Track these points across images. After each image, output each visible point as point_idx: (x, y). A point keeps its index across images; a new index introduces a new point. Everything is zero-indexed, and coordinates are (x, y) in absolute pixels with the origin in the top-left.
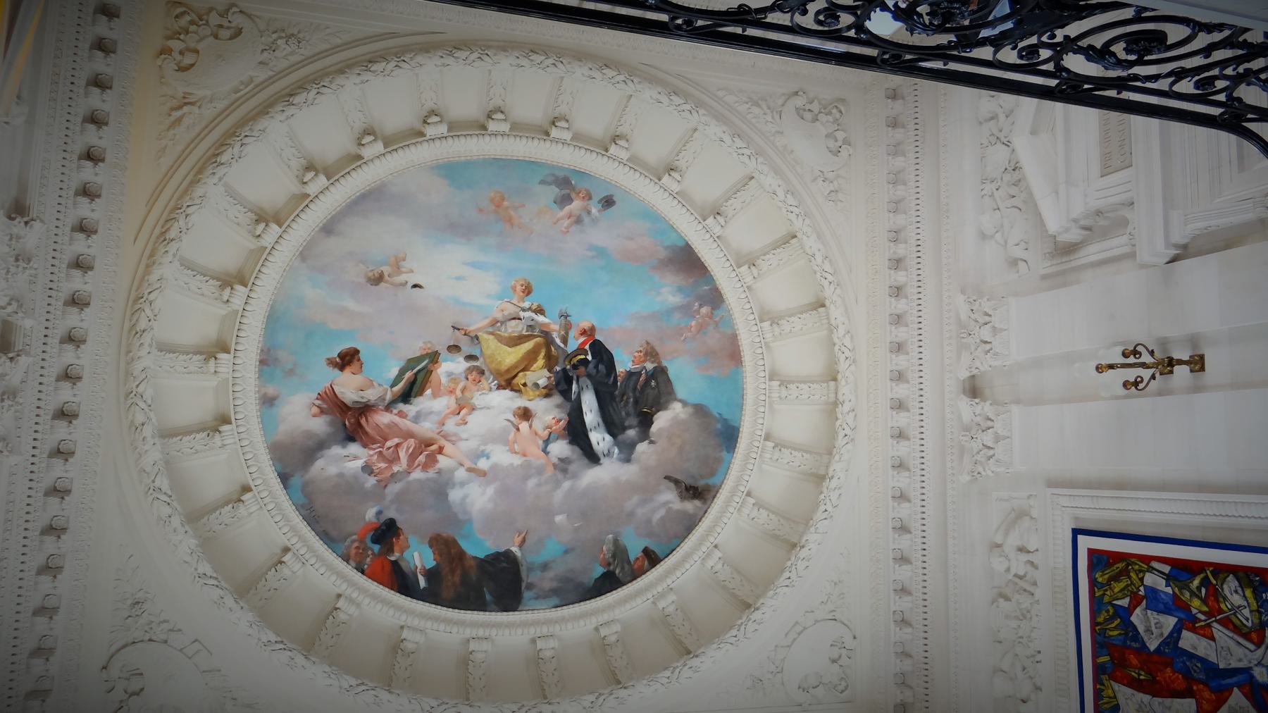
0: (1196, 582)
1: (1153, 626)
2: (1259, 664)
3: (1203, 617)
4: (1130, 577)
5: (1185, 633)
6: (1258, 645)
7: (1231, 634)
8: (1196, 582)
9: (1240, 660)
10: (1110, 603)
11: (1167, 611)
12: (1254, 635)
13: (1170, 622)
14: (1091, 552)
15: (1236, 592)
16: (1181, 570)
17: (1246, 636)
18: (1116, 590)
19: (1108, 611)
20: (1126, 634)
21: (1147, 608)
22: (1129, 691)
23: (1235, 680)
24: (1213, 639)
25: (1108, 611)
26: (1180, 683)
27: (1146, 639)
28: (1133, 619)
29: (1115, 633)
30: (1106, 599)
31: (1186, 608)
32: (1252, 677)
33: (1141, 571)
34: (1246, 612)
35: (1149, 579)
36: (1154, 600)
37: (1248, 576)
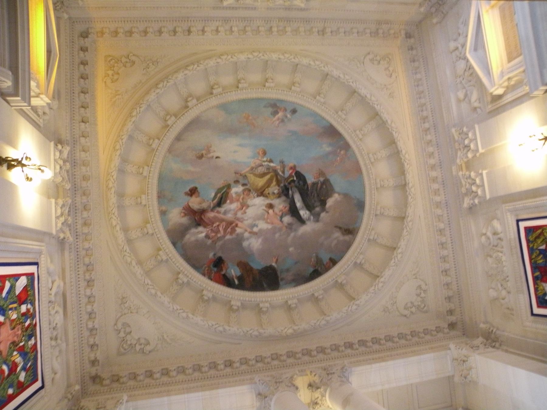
10: (537, 249)
18: (539, 242)
19: (536, 253)
30: (535, 247)
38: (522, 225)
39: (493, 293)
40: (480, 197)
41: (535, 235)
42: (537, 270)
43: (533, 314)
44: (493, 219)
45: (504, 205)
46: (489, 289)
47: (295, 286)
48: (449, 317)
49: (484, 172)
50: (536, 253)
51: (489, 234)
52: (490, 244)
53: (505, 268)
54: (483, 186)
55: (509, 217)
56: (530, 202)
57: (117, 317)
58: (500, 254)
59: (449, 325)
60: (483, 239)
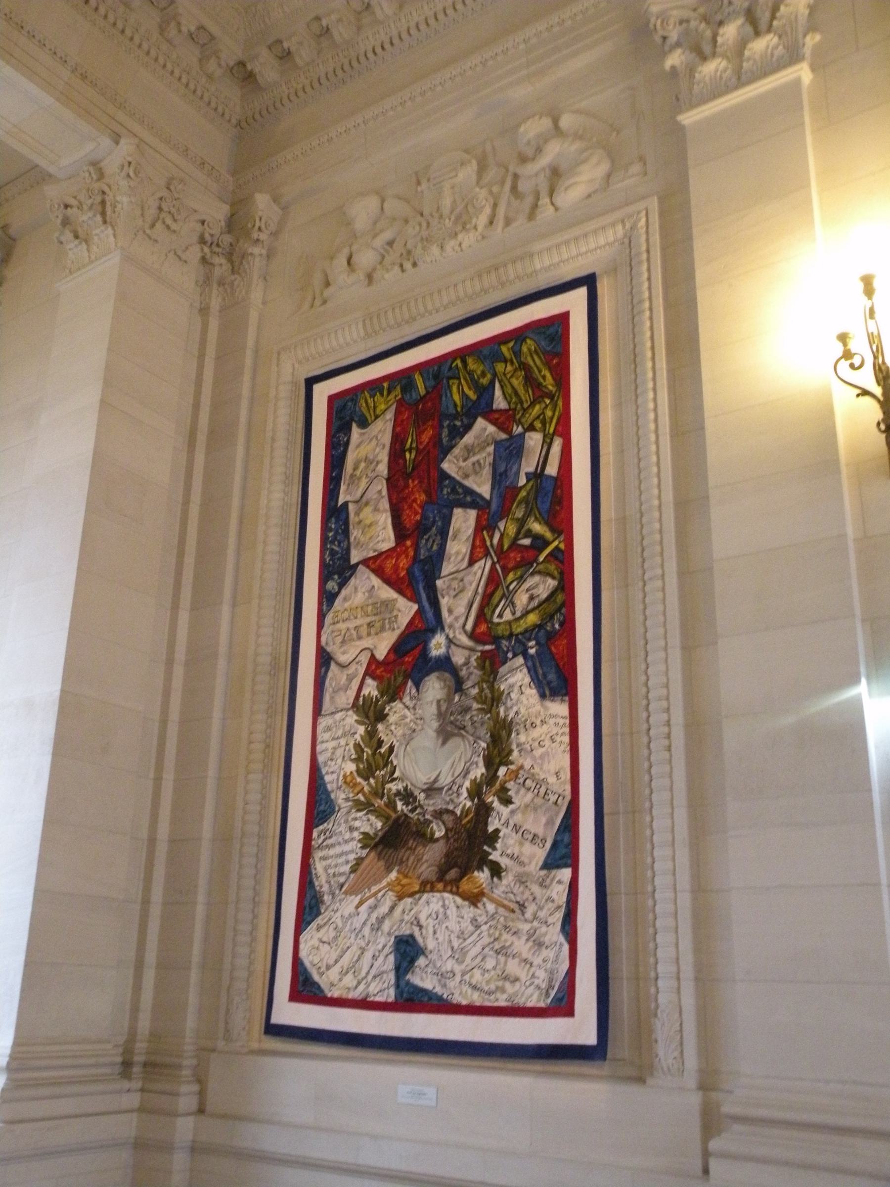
0: (537, 527)
1: (469, 463)
2: (450, 641)
3: (496, 540)
4: (533, 404)
5: (473, 514)
6: (472, 636)
7: (480, 590)
8: (537, 527)
9: (450, 611)
10: (495, 375)
11: (498, 478)
12: (483, 628)
13: (484, 489)
14: (563, 319)
15: (532, 598)
16: (553, 497)
17: (481, 617)
18: (515, 382)
19: (483, 374)
20: (456, 416)
21: (498, 444)
22: (387, 439)
23: (426, 604)
24: (472, 563)
25: (483, 374)
26: (411, 518)
27: (456, 451)
28: (480, 423)
29: (456, 398)
30: (500, 367)
31: (504, 512)
32: (433, 631)
33: (544, 423)
34: (508, 616)
35: (534, 440)
36: (510, 451)
37: (559, 610)
38: (574, 302)
39: (363, 212)
40: (691, 70)
41: (536, 362)
42: (432, 383)
43: (310, 382)
44: (612, 155)
45: (654, 204)
46: (377, 193)
48: (265, 53)
49: (803, 73)
51: (553, 151)
52: (523, 160)
53: (435, 250)
54: (741, 79)
55: (611, 235)
56: (655, 324)
59: (242, 64)
60: (533, 128)
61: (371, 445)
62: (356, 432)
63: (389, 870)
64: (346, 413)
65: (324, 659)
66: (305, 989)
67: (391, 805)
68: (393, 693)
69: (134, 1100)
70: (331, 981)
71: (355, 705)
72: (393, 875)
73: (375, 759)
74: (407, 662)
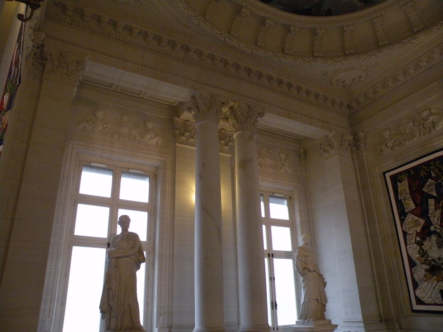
2: (435, 228)
6: (440, 226)
10: (430, 169)
21: (435, 184)
22: (407, 185)
24: (436, 210)
30: (431, 167)
43: (384, 173)
47: (282, 10)
50: (428, 169)
53: (408, 142)
57: (112, 311)
58: (418, 135)
61: (403, 186)
62: (399, 184)
63: (433, 276)
64: (395, 179)
65: (405, 234)
66: (419, 302)
67: (430, 262)
68: (424, 239)
69: (385, 327)
70: (425, 300)
71: (415, 243)
72: (435, 277)
73: (423, 253)
74: (425, 233)
